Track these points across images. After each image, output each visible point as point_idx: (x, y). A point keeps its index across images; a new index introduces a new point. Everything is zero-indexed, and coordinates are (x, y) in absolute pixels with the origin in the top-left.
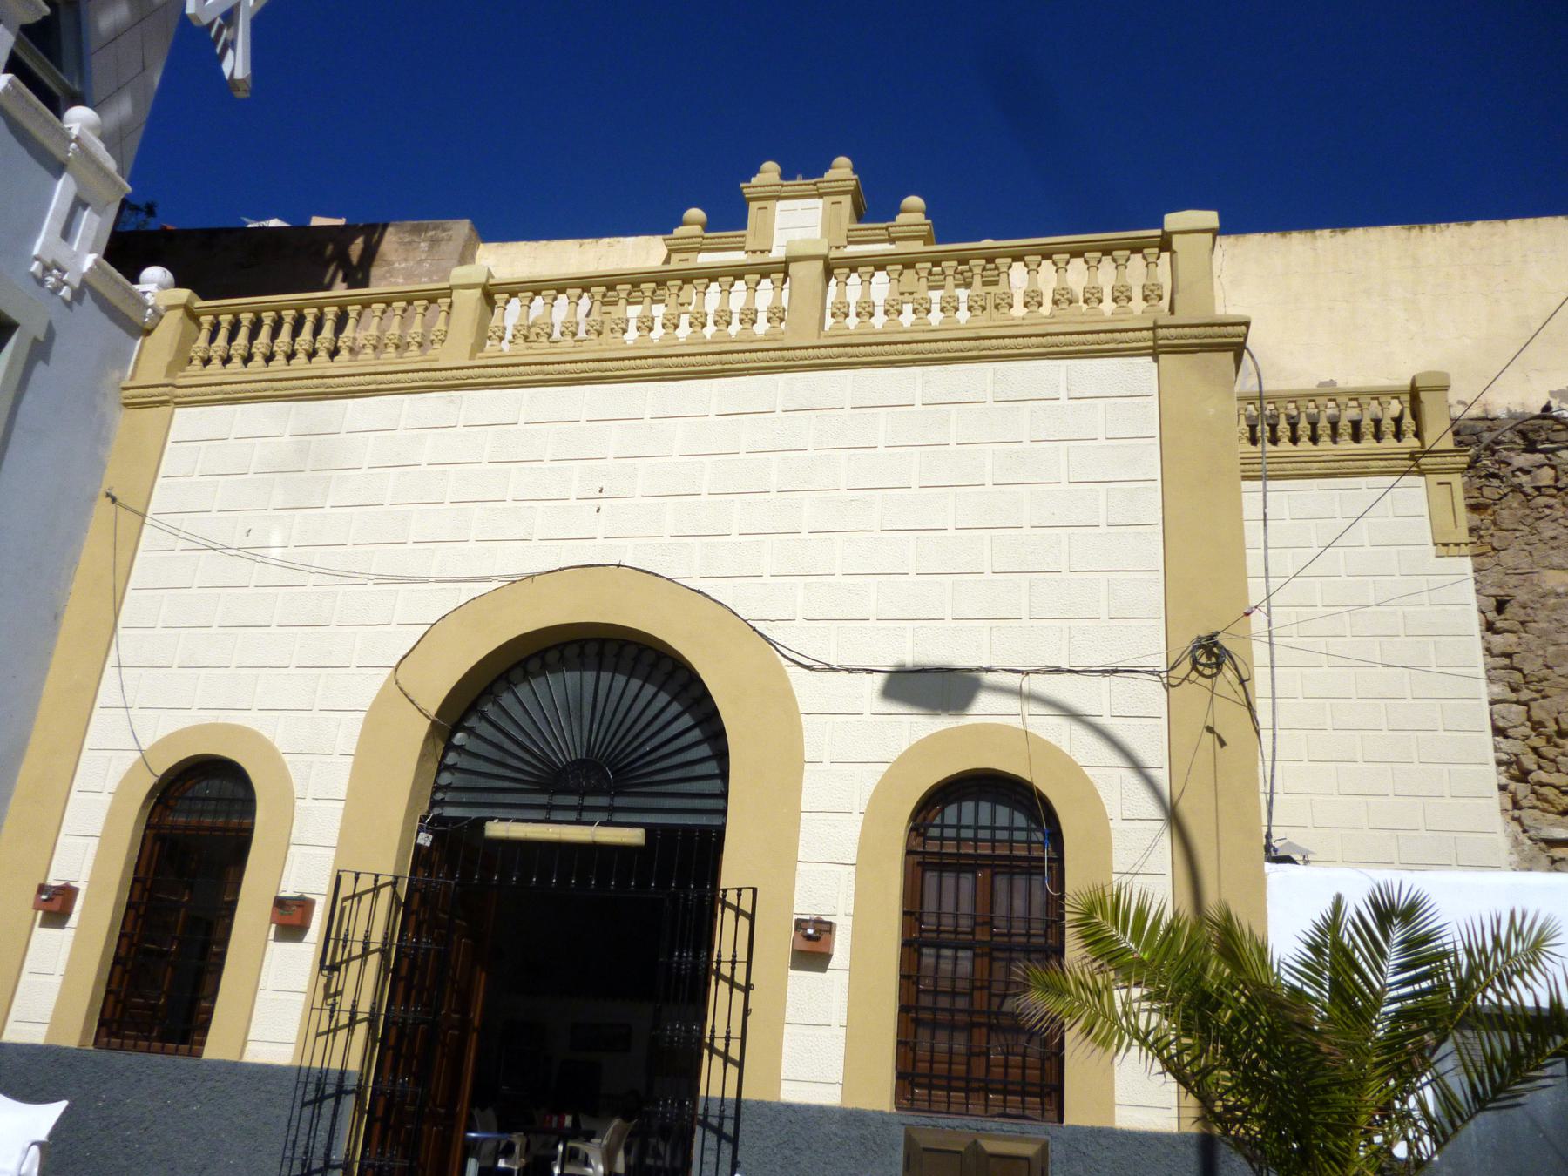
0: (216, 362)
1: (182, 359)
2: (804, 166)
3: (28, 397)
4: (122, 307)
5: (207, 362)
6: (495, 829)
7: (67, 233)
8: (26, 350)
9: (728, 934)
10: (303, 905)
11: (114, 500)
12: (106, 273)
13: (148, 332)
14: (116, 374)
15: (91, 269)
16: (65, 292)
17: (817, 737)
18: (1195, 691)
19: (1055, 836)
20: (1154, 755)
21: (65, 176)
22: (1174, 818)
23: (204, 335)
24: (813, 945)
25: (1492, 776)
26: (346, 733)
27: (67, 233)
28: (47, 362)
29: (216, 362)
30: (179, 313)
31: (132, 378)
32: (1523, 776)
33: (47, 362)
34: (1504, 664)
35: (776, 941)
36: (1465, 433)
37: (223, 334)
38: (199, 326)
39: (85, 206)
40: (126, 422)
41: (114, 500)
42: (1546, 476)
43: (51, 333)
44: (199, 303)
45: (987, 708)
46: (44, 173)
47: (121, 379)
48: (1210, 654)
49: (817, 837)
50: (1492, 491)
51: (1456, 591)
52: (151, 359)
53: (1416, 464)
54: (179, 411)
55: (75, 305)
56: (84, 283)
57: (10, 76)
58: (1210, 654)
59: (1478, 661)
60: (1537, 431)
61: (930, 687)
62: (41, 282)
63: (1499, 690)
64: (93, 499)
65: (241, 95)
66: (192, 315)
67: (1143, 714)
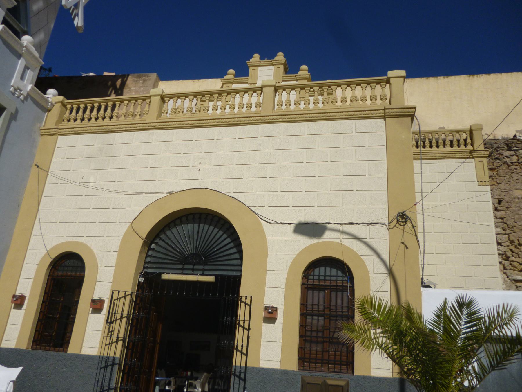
0: (72, 121)
1: (61, 120)
2: (268, 55)
3: (10, 132)
4: (41, 102)
5: (69, 121)
6: (165, 276)
7: (22, 78)
8: (8, 117)
9: (242, 311)
10: (101, 302)
11: (38, 167)
12: (35, 91)
13: (49, 111)
14: (39, 125)
15: (30, 90)
16: (22, 97)
17: (272, 246)
18: (398, 230)
19: (351, 279)
20: (384, 252)
21: (22, 59)
22: (391, 273)
23: (68, 112)
24: (271, 315)
25: (497, 259)
26: (115, 244)
27: (22, 78)
28: (16, 121)
29: (72, 121)
30: (60, 104)
31: (44, 126)
32: (507, 259)
33: (16, 121)
34: (501, 221)
35: (258, 314)
36: (488, 144)
37: (74, 112)
38: (66, 109)
39: (28, 69)
40: (42, 141)
41: (38, 167)
42: (515, 159)
43: (17, 111)
44: (66, 101)
45: (328, 236)
46: (14, 57)
47: (40, 126)
48: (403, 218)
49: (272, 279)
50: (497, 164)
51: (485, 197)
52: (50, 120)
53: (471, 155)
54: (59, 137)
55: (25, 102)
56: (28, 94)
57: (3, 25)
58: (403, 218)
59: (492, 220)
60: (512, 144)
61: (310, 229)
62: (13, 94)
63: (499, 230)
64: (31, 166)
65: (80, 32)
66: (64, 105)
67: (381, 238)
